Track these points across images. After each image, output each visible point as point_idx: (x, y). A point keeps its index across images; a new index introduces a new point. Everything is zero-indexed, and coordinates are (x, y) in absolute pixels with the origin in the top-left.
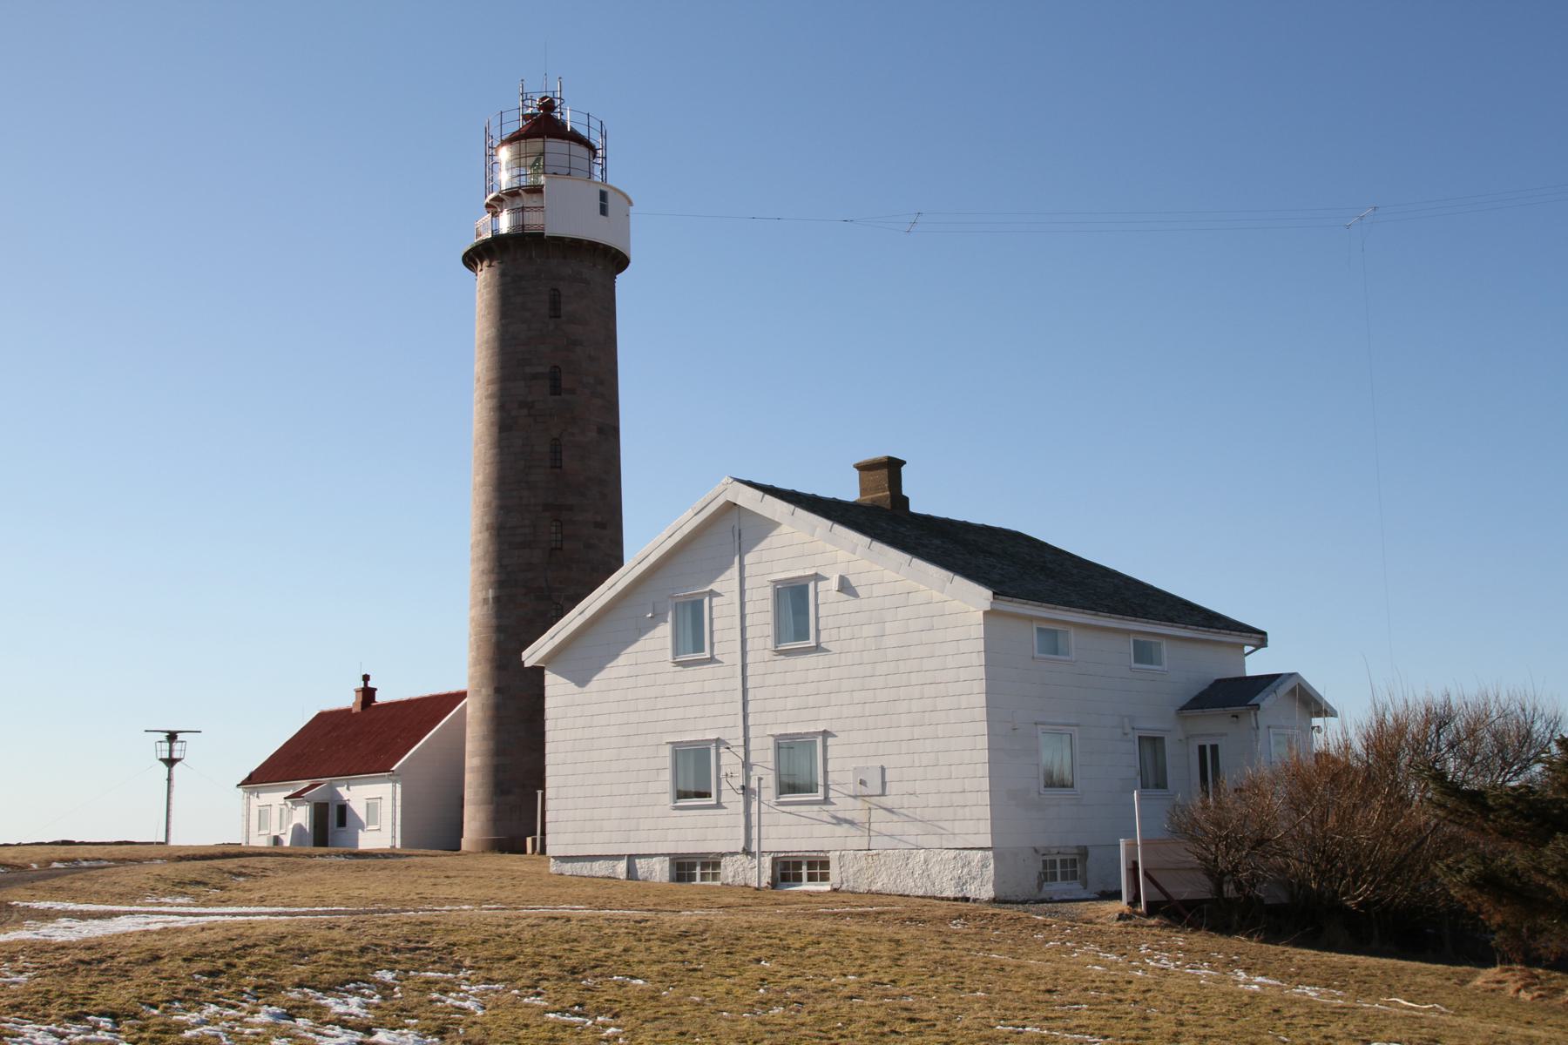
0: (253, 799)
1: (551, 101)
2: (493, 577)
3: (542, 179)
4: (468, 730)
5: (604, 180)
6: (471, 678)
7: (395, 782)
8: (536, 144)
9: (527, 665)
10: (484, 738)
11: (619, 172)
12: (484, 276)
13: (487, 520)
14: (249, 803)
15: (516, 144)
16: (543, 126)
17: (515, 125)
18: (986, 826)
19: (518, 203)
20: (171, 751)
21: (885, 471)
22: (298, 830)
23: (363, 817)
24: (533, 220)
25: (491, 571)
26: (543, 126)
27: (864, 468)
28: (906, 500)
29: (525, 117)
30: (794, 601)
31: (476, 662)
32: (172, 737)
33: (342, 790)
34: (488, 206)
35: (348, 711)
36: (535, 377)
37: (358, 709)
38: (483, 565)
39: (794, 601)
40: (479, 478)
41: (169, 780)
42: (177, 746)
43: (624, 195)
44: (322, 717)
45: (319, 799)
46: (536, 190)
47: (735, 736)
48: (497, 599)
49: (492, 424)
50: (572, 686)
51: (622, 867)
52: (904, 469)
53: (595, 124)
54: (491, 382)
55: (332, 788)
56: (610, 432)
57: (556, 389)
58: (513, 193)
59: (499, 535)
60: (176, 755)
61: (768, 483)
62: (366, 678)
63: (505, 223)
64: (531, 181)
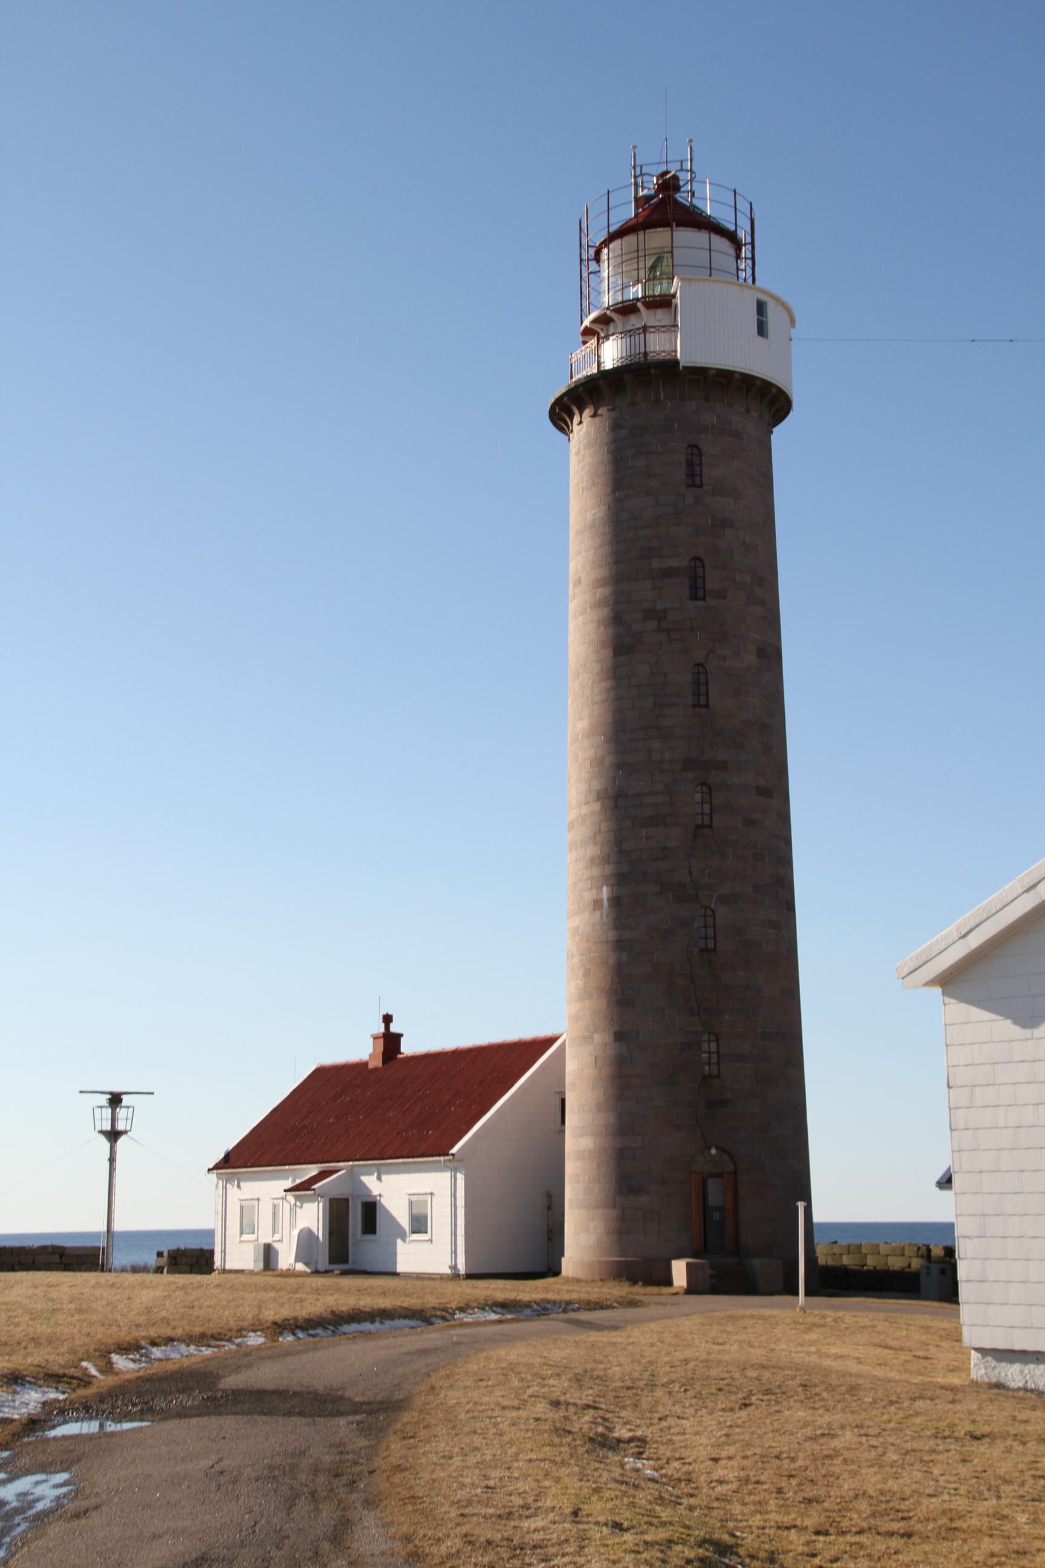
0: (232, 1190)
1: (675, 178)
2: (609, 869)
6: (575, 1019)
7: (454, 1170)
8: (657, 238)
10: (599, 1108)
13: (597, 785)
15: (630, 240)
16: (665, 208)
17: (627, 212)
19: (634, 322)
20: (114, 1120)
22: (306, 1239)
24: (657, 345)
25: (605, 860)
26: (665, 208)
31: (584, 995)
33: (370, 1182)
34: (588, 332)
36: (668, 573)
37: (378, 1062)
38: (592, 851)
40: (583, 725)
41: (112, 1160)
42: (121, 1113)
45: (339, 1192)
48: (616, 902)
49: (603, 644)
53: (743, 207)
54: (601, 583)
55: (353, 1178)
56: (770, 655)
57: (697, 591)
58: (627, 309)
59: (616, 807)
60: (120, 1126)
62: (388, 1019)
63: (611, 353)
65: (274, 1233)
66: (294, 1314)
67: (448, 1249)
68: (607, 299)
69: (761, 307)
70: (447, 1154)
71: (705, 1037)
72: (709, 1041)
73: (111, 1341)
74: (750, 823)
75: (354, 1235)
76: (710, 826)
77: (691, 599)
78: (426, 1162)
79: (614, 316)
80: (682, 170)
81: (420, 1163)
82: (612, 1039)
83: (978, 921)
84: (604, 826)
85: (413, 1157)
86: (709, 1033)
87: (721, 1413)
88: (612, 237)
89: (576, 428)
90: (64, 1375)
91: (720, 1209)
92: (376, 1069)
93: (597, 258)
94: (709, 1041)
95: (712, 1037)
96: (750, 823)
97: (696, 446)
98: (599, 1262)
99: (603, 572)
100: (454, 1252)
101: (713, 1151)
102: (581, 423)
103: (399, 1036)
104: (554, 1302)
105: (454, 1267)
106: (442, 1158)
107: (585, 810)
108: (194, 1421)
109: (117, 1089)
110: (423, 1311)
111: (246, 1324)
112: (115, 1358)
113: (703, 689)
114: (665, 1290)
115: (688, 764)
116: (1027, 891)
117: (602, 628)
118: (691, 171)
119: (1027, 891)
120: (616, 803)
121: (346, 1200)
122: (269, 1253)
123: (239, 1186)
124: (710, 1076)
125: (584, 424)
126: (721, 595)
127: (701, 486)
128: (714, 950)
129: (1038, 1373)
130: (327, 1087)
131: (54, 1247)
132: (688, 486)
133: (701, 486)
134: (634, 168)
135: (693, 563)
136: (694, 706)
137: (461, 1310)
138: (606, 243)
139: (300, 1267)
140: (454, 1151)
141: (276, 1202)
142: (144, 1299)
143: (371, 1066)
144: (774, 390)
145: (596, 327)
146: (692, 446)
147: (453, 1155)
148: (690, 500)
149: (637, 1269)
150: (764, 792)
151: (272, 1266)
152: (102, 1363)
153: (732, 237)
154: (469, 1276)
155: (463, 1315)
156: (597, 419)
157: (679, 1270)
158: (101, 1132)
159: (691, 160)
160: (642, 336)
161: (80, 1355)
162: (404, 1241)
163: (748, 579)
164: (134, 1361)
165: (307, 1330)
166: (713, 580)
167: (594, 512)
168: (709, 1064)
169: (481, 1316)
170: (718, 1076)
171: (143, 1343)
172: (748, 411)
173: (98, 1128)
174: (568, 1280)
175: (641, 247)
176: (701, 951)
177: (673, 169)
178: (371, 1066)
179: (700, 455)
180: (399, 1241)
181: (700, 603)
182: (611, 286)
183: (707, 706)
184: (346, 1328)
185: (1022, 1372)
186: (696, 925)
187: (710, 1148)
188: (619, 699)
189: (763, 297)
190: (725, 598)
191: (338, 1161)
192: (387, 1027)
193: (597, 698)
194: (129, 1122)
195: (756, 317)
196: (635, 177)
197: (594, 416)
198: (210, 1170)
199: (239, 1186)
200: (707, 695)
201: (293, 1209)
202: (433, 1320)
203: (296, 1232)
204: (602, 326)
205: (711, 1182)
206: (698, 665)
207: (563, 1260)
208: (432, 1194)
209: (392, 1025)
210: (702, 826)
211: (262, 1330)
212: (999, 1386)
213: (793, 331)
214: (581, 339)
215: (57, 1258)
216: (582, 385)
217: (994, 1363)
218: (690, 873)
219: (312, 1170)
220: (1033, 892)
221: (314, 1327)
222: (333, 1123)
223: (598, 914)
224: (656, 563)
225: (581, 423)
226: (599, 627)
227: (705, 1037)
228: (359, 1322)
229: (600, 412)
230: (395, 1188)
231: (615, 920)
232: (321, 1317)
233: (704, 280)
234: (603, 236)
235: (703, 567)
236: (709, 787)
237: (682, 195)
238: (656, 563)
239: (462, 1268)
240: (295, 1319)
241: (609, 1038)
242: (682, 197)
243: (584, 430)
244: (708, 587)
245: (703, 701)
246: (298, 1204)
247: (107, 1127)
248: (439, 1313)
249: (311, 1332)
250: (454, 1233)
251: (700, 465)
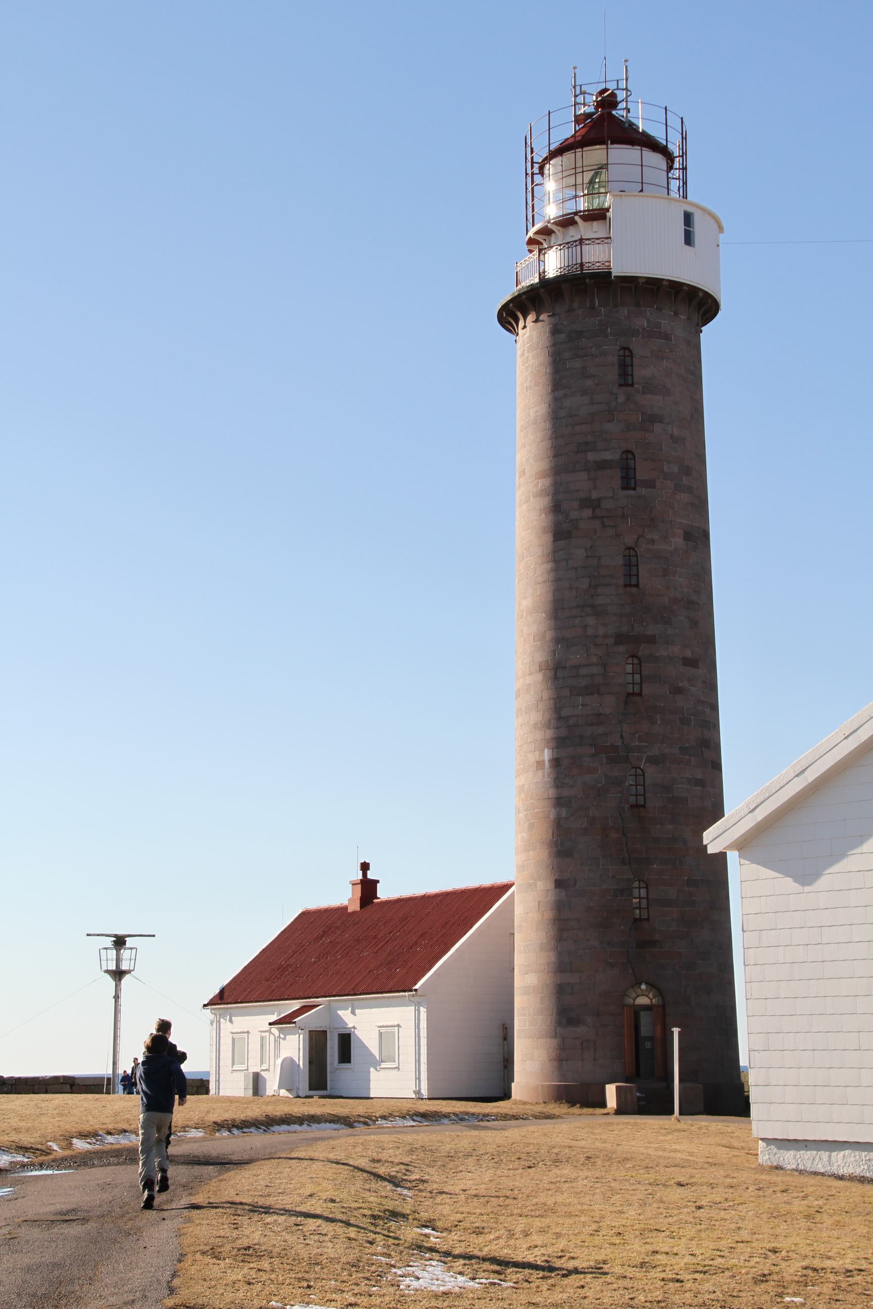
1: (613, 95)
2: (550, 734)
3: (608, 201)
4: (518, 937)
6: (521, 868)
7: (418, 1005)
8: (595, 154)
9: (710, 851)
13: (540, 657)
14: (219, 1029)
15: (568, 157)
16: (604, 125)
17: (567, 131)
19: (573, 234)
20: (118, 960)
22: (289, 1066)
23: (375, 1051)
24: (594, 256)
25: (548, 725)
26: (604, 125)
29: (578, 119)
32: (120, 942)
33: (345, 1015)
34: (531, 242)
35: (343, 910)
36: (601, 465)
37: (355, 907)
38: (536, 717)
40: (527, 603)
41: (117, 997)
42: (125, 954)
44: (306, 916)
45: (318, 1025)
46: (598, 215)
48: (556, 762)
50: (788, 884)
53: (674, 122)
54: (542, 475)
57: (628, 481)
58: (567, 222)
59: (555, 678)
60: (124, 967)
62: (365, 867)
63: (553, 263)
64: (582, 205)
65: (262, 1063)
66: (234, 1116)
67: (413, 1076)
68: (552, 212)
69: (688, 218)
70: (411, 991)
71: (636, 884)
72: (639, 888)
73: (75, 1130)
74: (678, 691)
75: (332, 1064)
76: (640, 694)
77: (623, 489)
78: (393, 997)
79: (554, 228)
80: (618, 89)
81: (388, 998)
82: (553, 886)
83: (762, 799)
84: (546, 695)
85: (382, 993)
86: (640, 881)
88: (553, 154)
89: (521, 331)
90: (32, 1148)
91: (651, 1039)
92: (354, 913)
93: (541, 172)
94: (639, 888)
95: (642, 885)
96: (678, 691)
97: (628, 349)
98: (543, 1086)
99: (545, 465)
100: (418, 1079)
101: (643, 987)
102: (525, 327)
103: (376, 882)
104: (473, 1114)
105: (418, 1092)
106: (406, 994)
107: (529, 680)
109: (120, 932)
110: (348, 1117)
111: (191, 1123)
112: (75, 1141)
113: (634, 571)
114: (599, 1111)
115: (620, 639)
116: (797, 776)
117: (543, 516)
118: (626, 89)
119: (797, 776)
120: (556, 674)
121: (325, 1032)
122: (257, 1082)
123: (231, 1021)
124: (640, 919)
125: (528, 328)
126: (650, 484)
127: (632, 385)
128: (644, 806)
129: (806, 1157)
130: (313, 928)
131: (65, 1078)
132: (620, 385)
133: (632, 385)
134: (575, 87)
135: (624, 456)
136: (626, 586)
137: (384, 1117)
138: (547, 160)
139: (283, 1093)
140: (416, 987)
141: (263, 1034)
142: (116, 1107)
143: (350, 910)
144: (701, 294)
145: (539, 238)
146: (624, 349)
147: (416, 990)
148: (621, 399)
149: (579, 1094)
150: (691, 663)
151: (260, 1092)
152: (64, 1144)
153: (669, 157)
154: (429, 1099)
155: (384, 1122)
156: (539, 324)
157: (611, 1091)
158: (107, 971)
159: (627, 80)
160: (579, 247)
161: (49, 1138)
162: (376, 1069)
163: (675, 469)
164: (90, 1144)
165: (242, 1128)
166: (642, 472)
167: (536, 409)
168: (640, 908)
169: (400, 1122)
170: (648, 919)
171: (101, 1133)
172: (676, 314)
173: (105, 968)
174: (516, 1102)
175: (579, 164)
176: (632, 806)
177: (612, 86)
178: (350, 910)
179: (632, 356)
180: (372, 1069)
181: (631, 492)
182: (553, 199)
183: (637, 586)
184: (276, 1128)
185: (795, 1156)
186: (627, 784)
187: (641, 984)
188: (557, 580)
189: (690, 209)
190: (654, 487)
191: (317, 997)
192: (365, 875)
193: (540, 579)
194: (133, 962)
195: (683, 227)
196: (576, 96)
197: (536, 321)
198: (205, 1005)
199: (231, 1021)
200: (637, 575)
201: (277, 1041)
202: (356, 1124)
203: (279, 1061)
204: (544, 237)
205: (642, 1014)
206: (629, 548)
207: (513, 1085)
208: (399, 1026)
209: (368, 872)
210: (633, 694)
211: (203, 1128)
212: (778, 1168)
213: (721, 235)
214: (526, 248)
215: (72, 1086)
216: (524, 293)
217: (775, 1150)
218: (622, 737)
219: (296, 1005)
220: (802, 776)
221: (247, 1127)
222: (315, 962)
223: (540, 773)
224: (591, 456)
225: (525, 327)
226: (540, 515)
227: (636, 884)
228: (289, 1124)
229: (541, 318)
231: (555, 779)
232: (256, 1120)
233: (634, 196)
234: (545, 153)
235: (634, 459)
236: (639, 659)
237: (619, 112)
238: (591, 456)
239: (425, 1092)
240: (234, 1120)
241: (550, 885)
242: (619, 113)
243: (528, 333)
244: (637, 478)
245: (634, 582)
246: (282, 1036)
248: (362, 1119)
249: (245, 1130)
250: (418, 1061)
251: (632, 365)
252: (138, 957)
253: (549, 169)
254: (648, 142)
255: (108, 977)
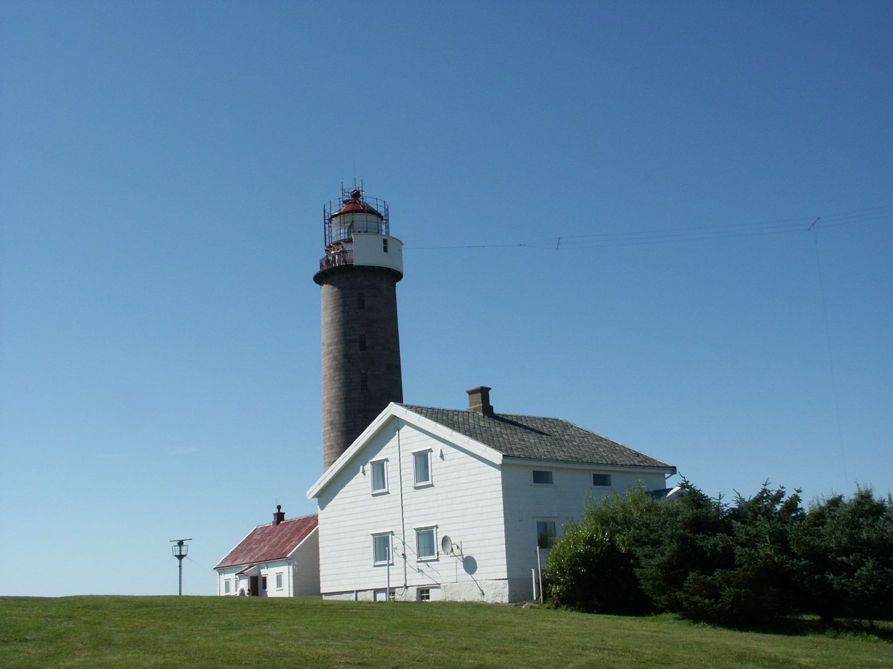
1: (358, 192)
5: (388, 233)
11: (396, 229)
12: (326, 290)
18: (505, 568)
20: (180, 551)
21: (479, 395)
27: (471, 393)
28: (492, 407)
30: (422, 459)
32: (181, 543)
39: (422, 459)
41: (180, 567)
42: (183, 548)
43: (399, 241)
45: (254, 574)
47: (398, 530)
51: (354, 595)
52: (490, 392)
57: (363, 347)
60: (183, 553)
61: (417, 404)
62: (279, 507)
69: (385, 241)
87: (589, 645)
99: (335, 340)
108: (810, 637)
153: (379, 215)
182: (338, 233)
230: (270, 573)
247: (178, 554)
252: (190, 549)
253: (335, 220)
254: (372, 212)
255: (176, 558)
